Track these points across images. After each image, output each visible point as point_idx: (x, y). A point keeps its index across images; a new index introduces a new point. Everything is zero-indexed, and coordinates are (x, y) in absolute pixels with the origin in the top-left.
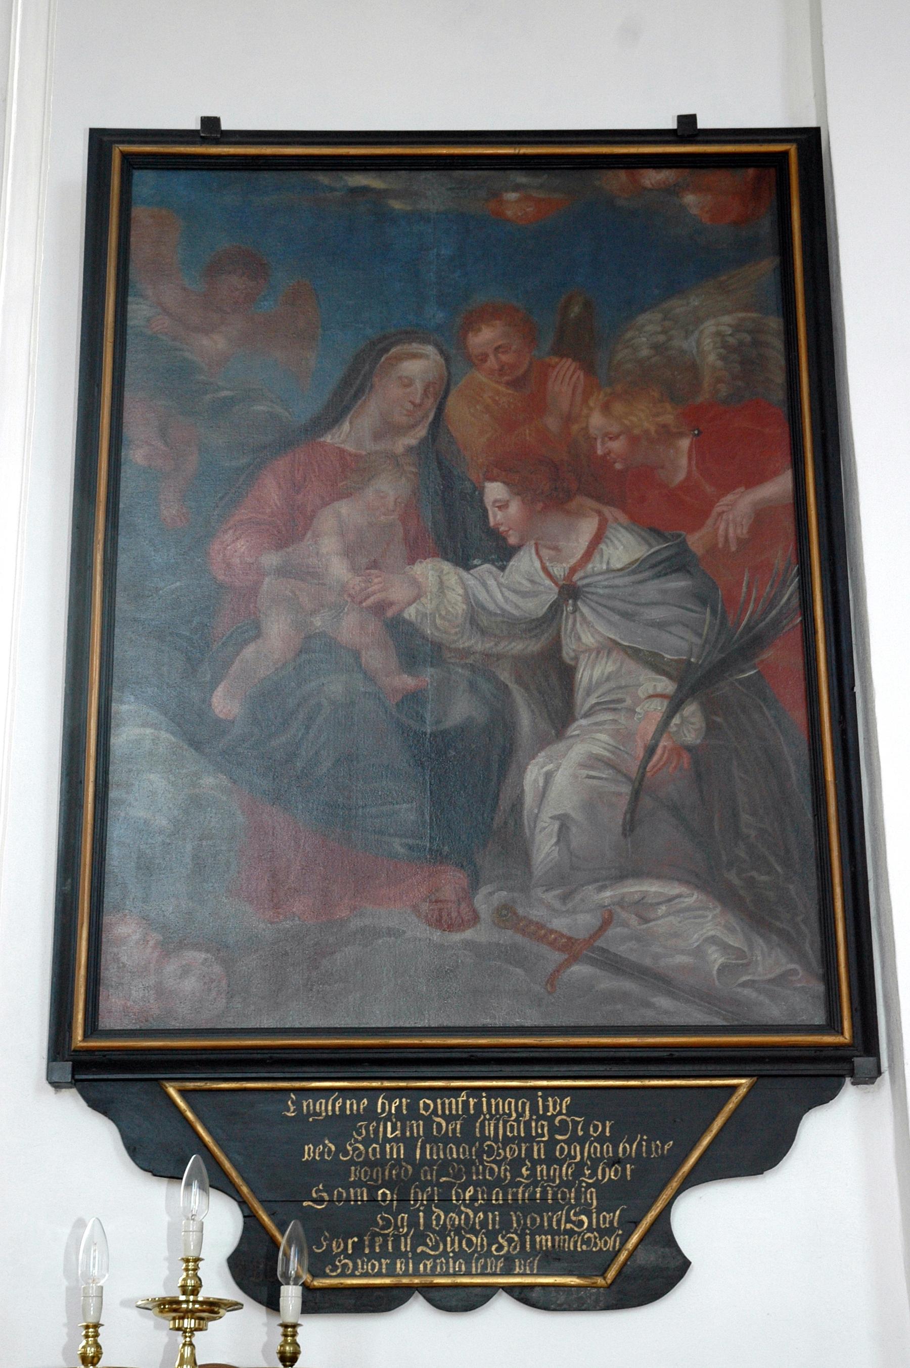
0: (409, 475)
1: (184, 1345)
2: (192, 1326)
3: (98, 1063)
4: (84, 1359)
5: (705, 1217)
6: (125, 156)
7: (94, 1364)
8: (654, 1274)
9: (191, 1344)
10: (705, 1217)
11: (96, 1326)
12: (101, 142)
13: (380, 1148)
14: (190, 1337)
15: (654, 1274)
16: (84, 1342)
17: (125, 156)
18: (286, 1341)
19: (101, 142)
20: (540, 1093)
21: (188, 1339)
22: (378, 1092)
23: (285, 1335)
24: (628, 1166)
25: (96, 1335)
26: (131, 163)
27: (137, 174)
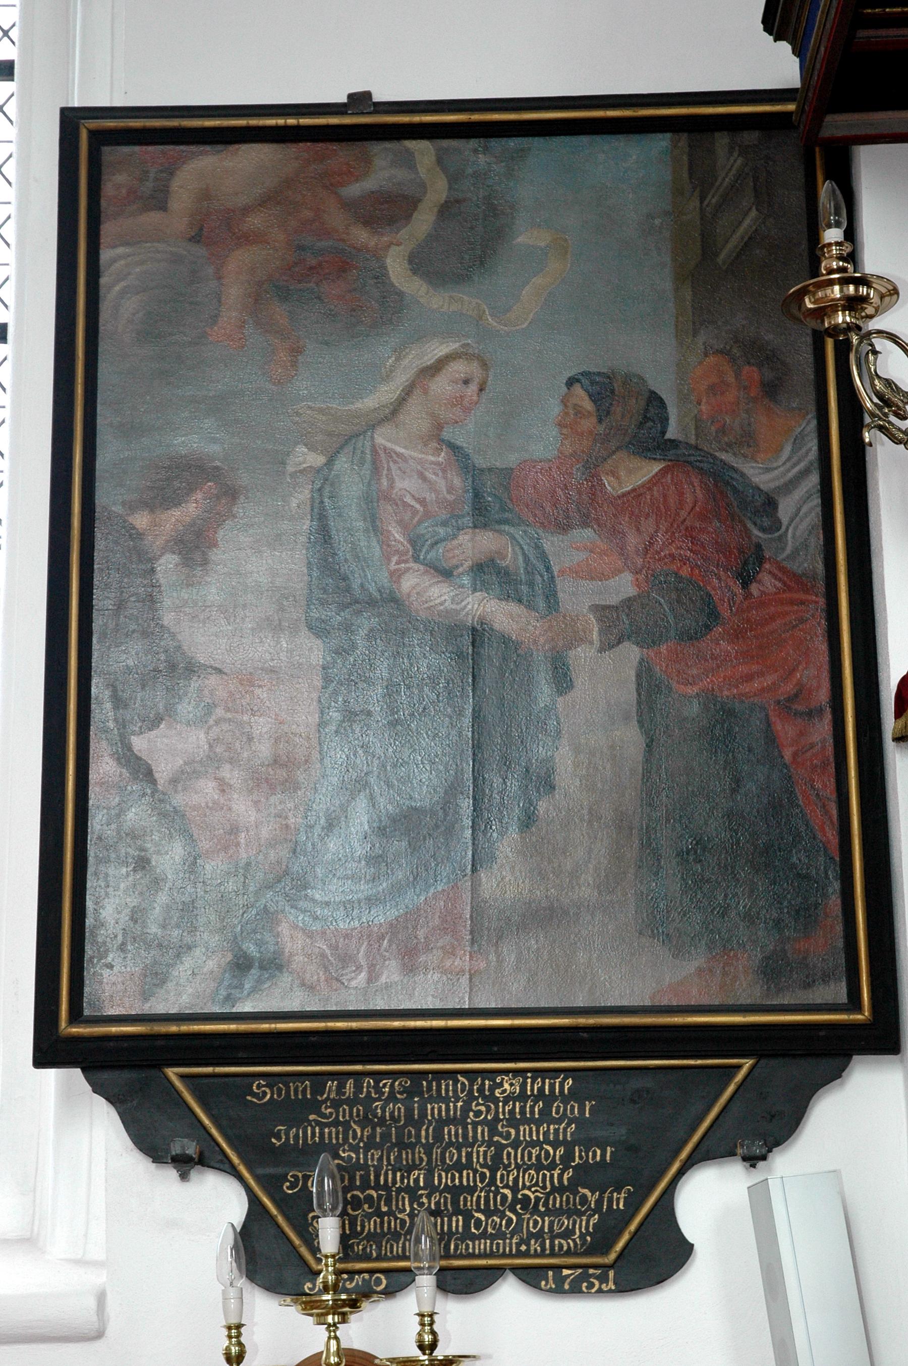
0: (775, 776)
1: (329, 1338)
2: (336, 1320)
3: (159, 1077)
4: (228, 1358)
5: (708, 1199)
6: (92, 133)
7: (239, 1363)
8: (652, 1256)
9: (336, 1338)
10: (708, 1199)
11: (239, 1327)
12: (70, 119)
13: (348, 1139)
14: (334, 1331)
15: (652, 1256)
16: (227, 1343)
17: (92, 133)
18: (423, 1330)
19: (70, 119)
20: (529, 1075)
21: (332, 1334)
22: (326, 1078)
23: (422, 1324)
24: (609, 1148)
25: (239, 1335)
26: (100, 138)
27: (106, 150)
